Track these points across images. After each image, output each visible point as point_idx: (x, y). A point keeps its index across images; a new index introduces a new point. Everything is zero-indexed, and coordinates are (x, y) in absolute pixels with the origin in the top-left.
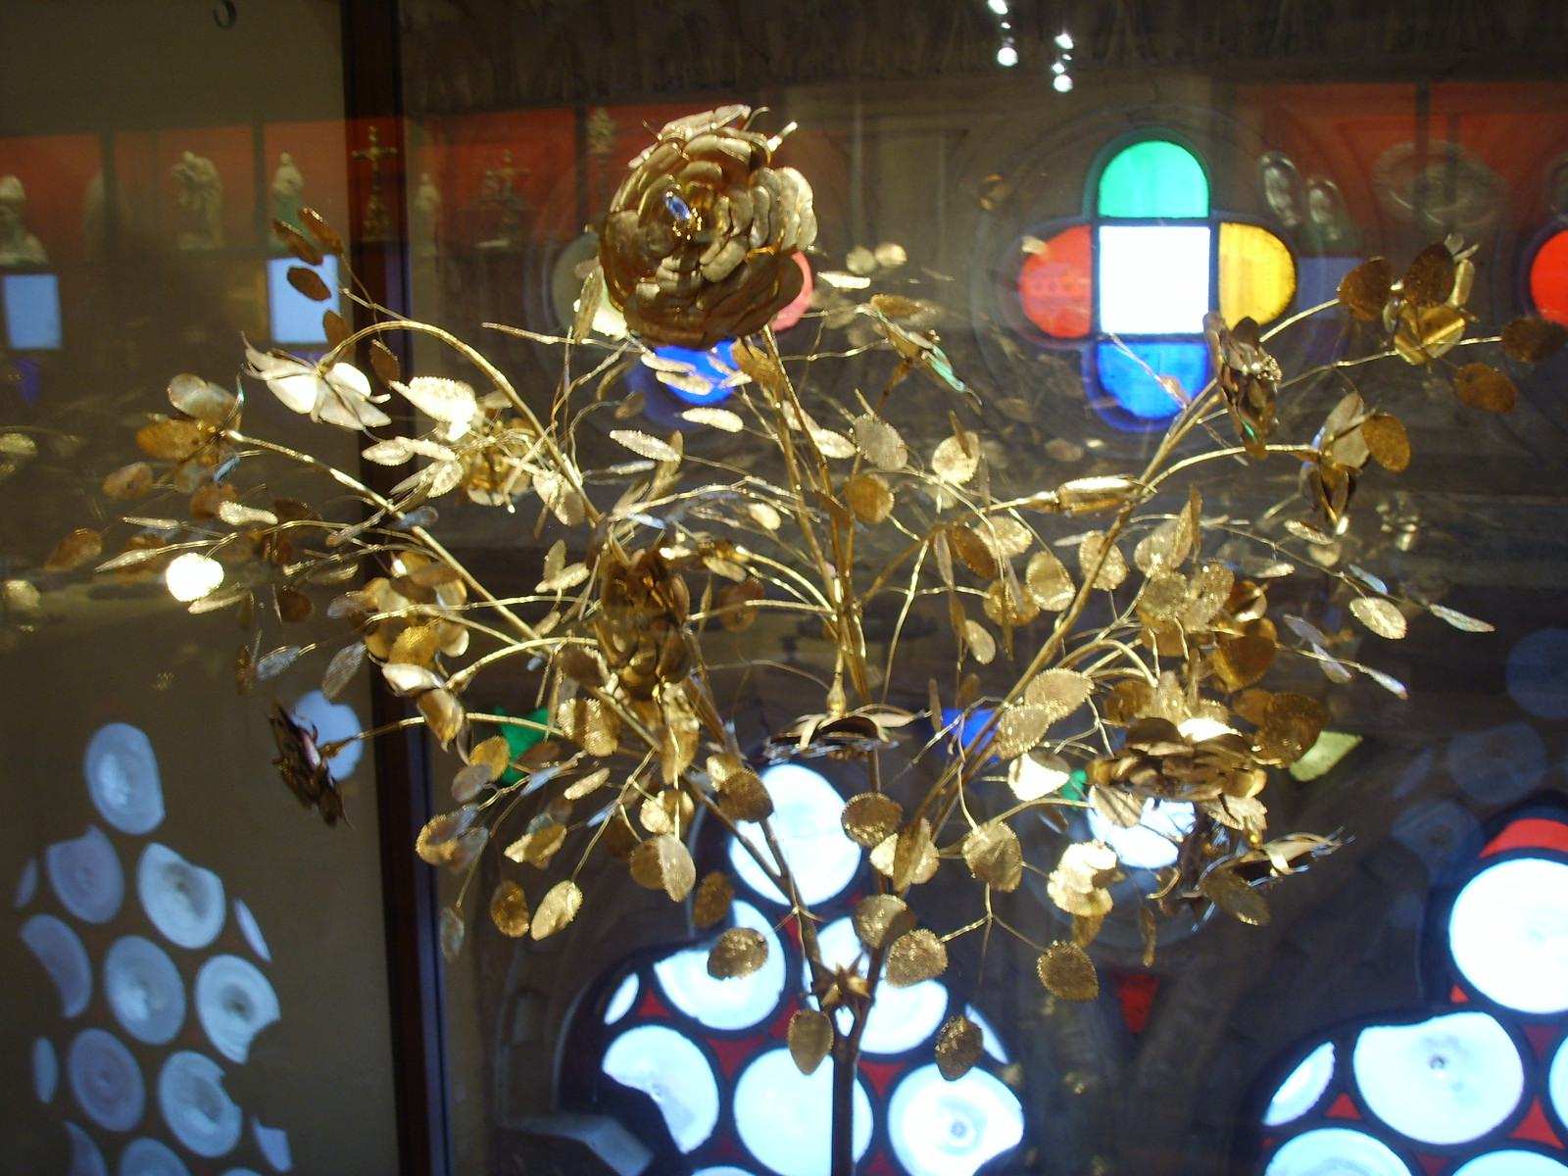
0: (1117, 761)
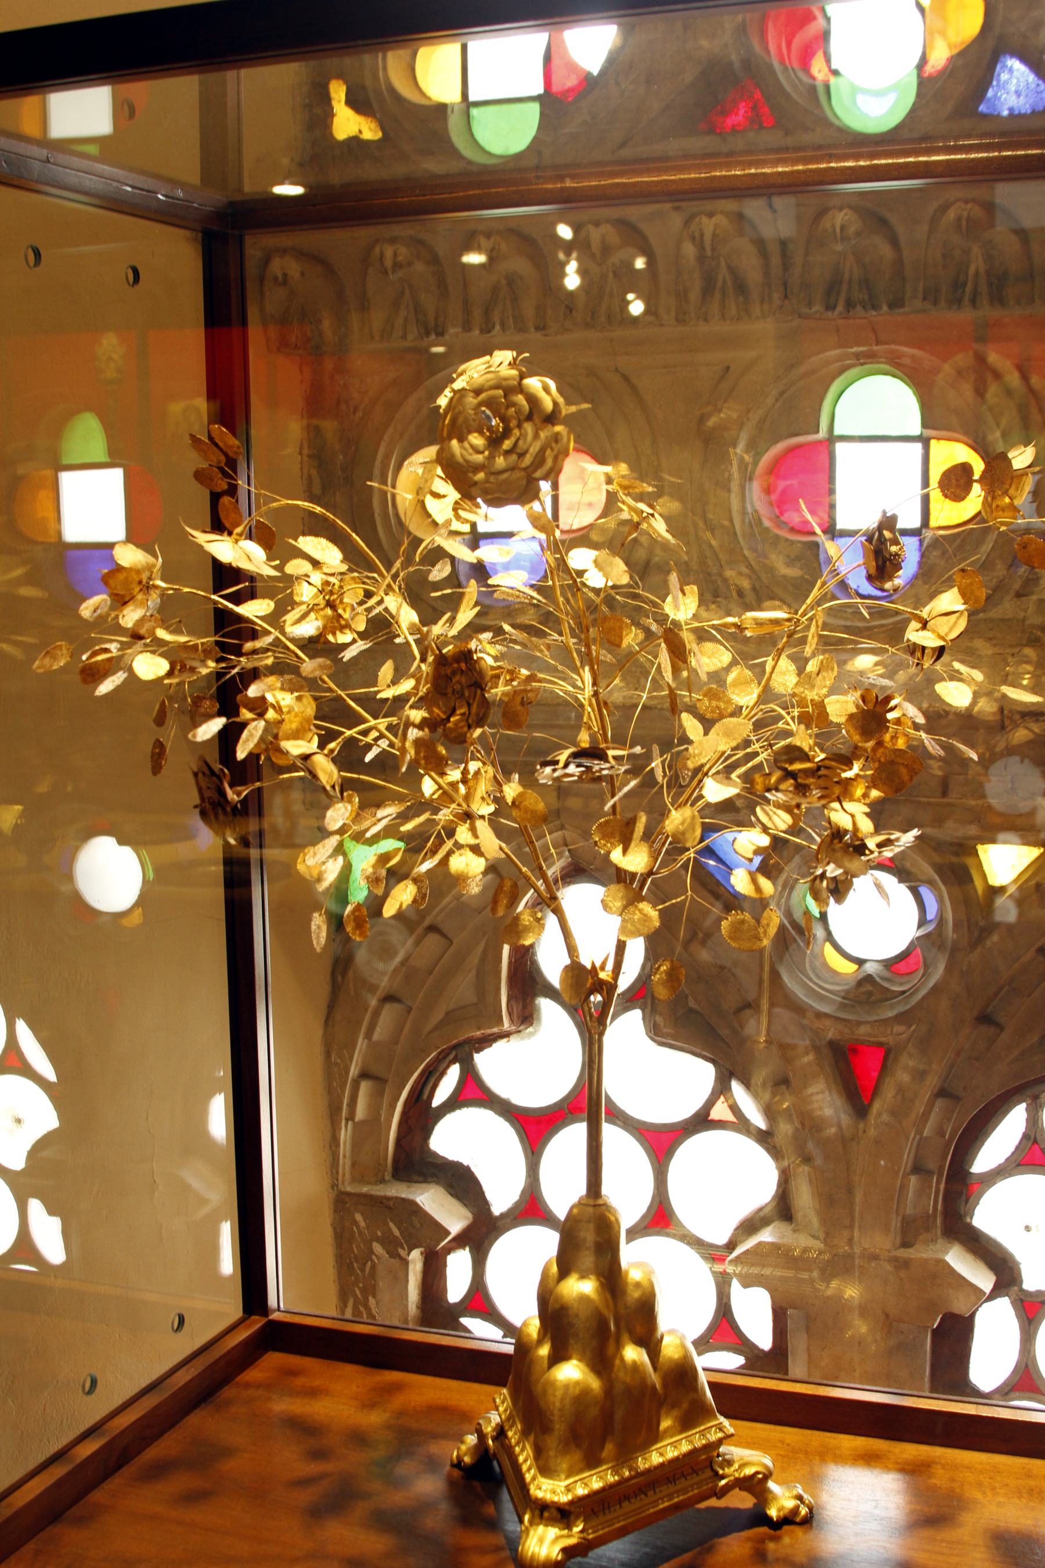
0: (769, 774)
